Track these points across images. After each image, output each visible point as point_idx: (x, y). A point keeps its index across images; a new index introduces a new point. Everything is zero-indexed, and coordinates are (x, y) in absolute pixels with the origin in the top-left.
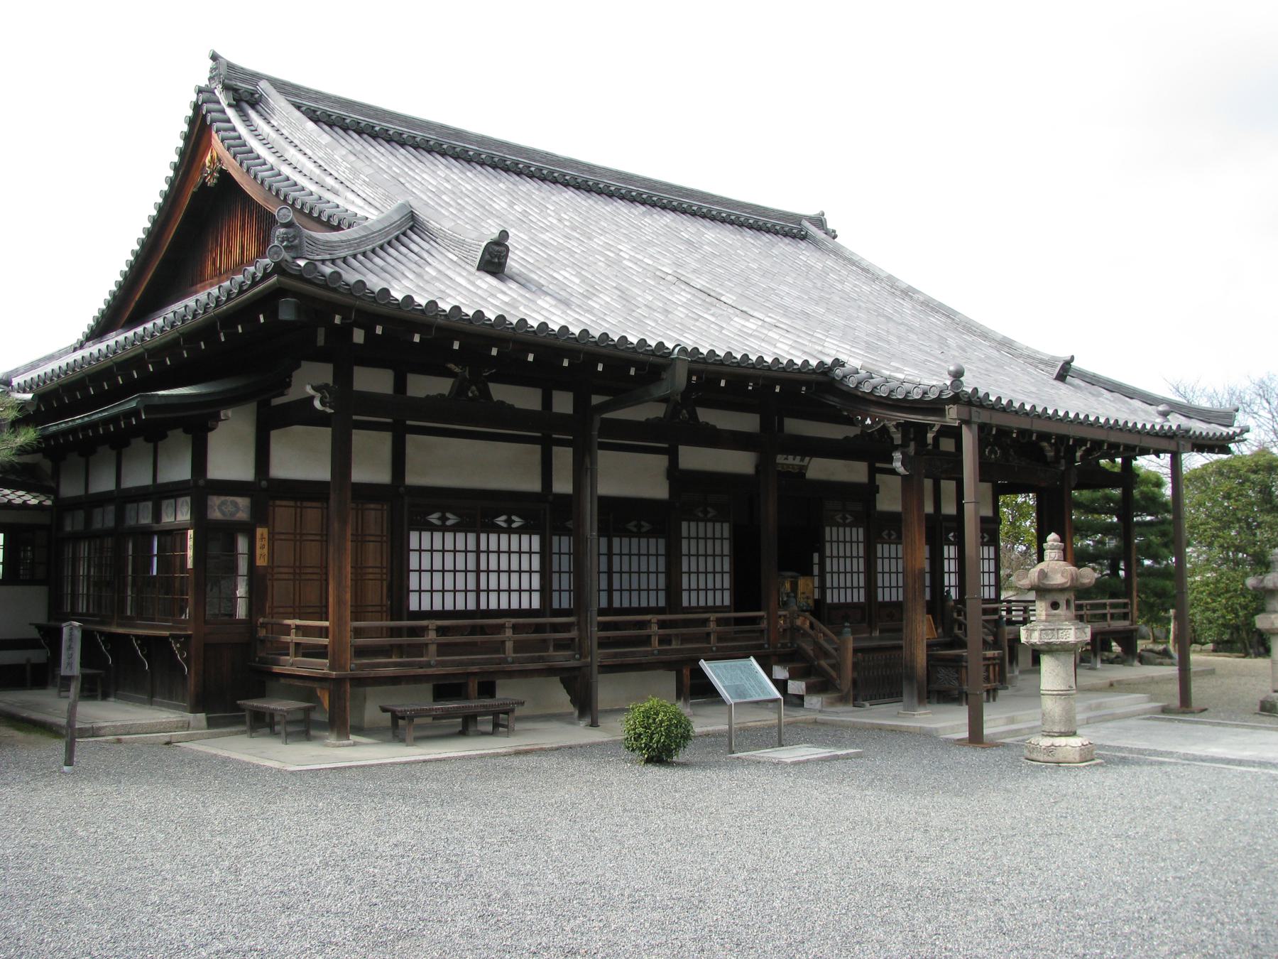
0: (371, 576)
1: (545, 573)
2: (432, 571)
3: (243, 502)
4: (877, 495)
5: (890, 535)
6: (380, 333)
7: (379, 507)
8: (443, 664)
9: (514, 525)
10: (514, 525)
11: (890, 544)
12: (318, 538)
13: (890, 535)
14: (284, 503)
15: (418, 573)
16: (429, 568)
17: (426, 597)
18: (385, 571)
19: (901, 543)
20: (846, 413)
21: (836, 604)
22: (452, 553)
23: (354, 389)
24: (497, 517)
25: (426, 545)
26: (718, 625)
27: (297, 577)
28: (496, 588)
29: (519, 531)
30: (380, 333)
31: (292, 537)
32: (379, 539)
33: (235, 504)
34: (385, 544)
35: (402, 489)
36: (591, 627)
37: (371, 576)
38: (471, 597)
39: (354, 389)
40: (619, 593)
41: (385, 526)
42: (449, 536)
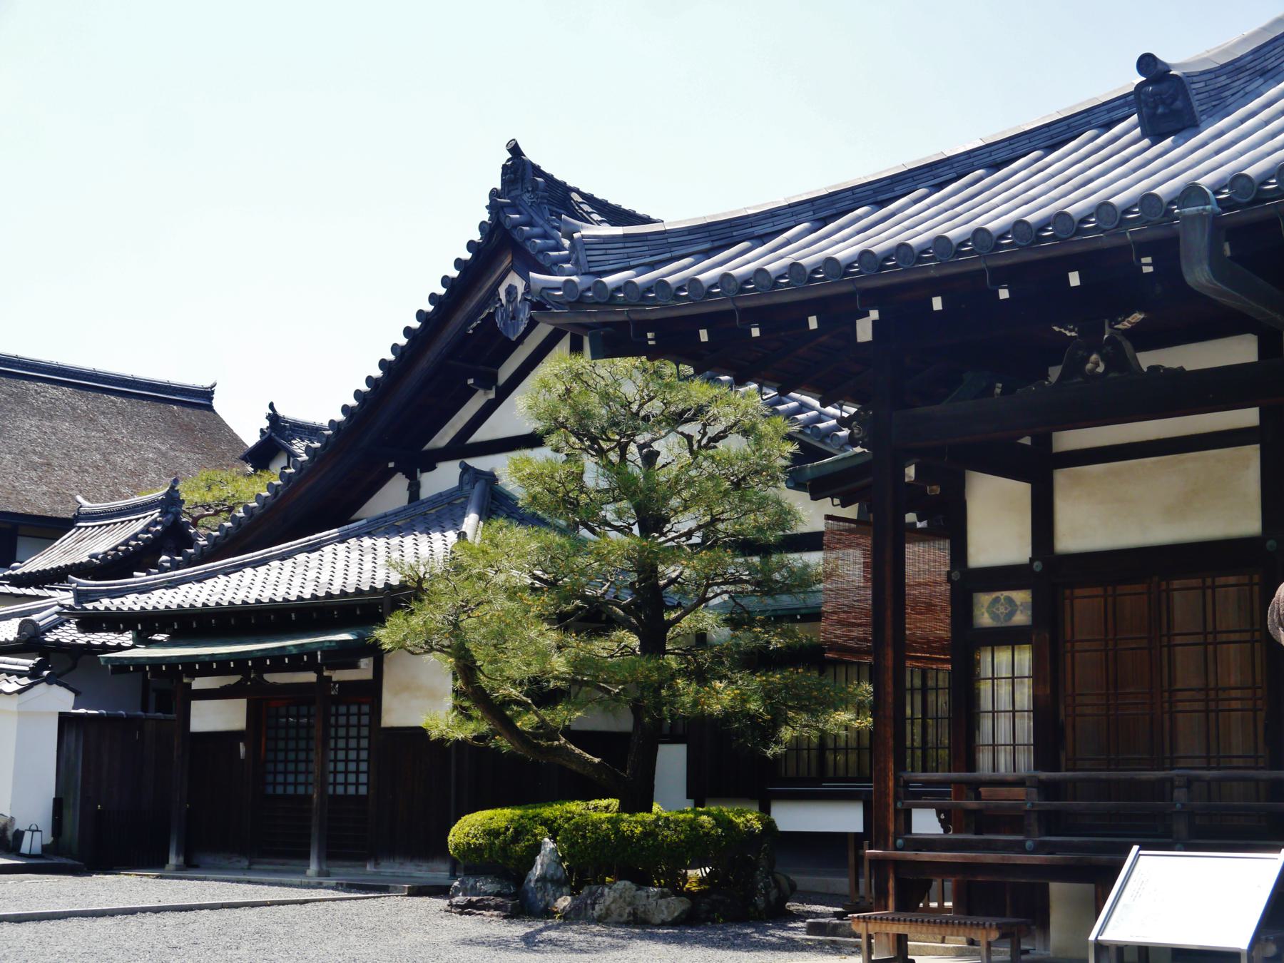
0: (1187, 706)
3: (1021, 597)
6: (1071, 274)
7: (1245, 579)
12: (1224, 637)
14: (1087, 592)
18: (1259, 692)
20: (1227, 247)
23: (192, 702)
27: (1212, 705)
30: (1071, 274)
31: (1200, 638)
32: (1247, 636)
33: (1010, 601)
34: (1257, 645)
36: (900, 766)
37: (1187, 706)
39: (192, 702)
41: (1068, 618)
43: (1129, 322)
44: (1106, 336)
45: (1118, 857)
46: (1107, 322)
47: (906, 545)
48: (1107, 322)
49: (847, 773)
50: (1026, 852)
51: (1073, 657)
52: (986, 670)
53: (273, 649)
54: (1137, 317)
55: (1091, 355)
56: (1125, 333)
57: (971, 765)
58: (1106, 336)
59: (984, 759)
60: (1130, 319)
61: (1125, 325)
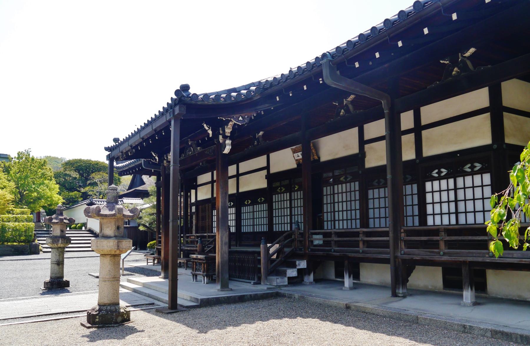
1: (422, 204)
2: (380, 208)
4: (266, 174)
5: (379, 183)
8: (450, 254)
9: (443, 174)
10: (443, 174)
11: (379, 188)
13: (379, 183)
15: (472, 201)
16: (481, 197)
17: (438, 218)
19: (386, 187)
21: (277, 231)
22: (475, 188)
24: (433, 172)
25: (376, 196)
26: (407, 236)
28: (384, 216)
29: (446, 177)
35: (495, 146)
38: (453, 217)
40: (432, 216)
42: (444, 182)
43: (350, 98)
44: (460, 60)
45: (215, 268)
46: (460, 54)
47: (156, 212)
48: (460, 54)
49: (152, 262)
50: (360, 253)
51: (331, 201)
52: (370, 196)
53: (216, 212)
54: (472, 50)
55: (454, 69)
56: (469, 58)
57: (367, 226)
58: (460, 60)
59: (371, 224)
60: (350, 97)
61: (468, 54)
